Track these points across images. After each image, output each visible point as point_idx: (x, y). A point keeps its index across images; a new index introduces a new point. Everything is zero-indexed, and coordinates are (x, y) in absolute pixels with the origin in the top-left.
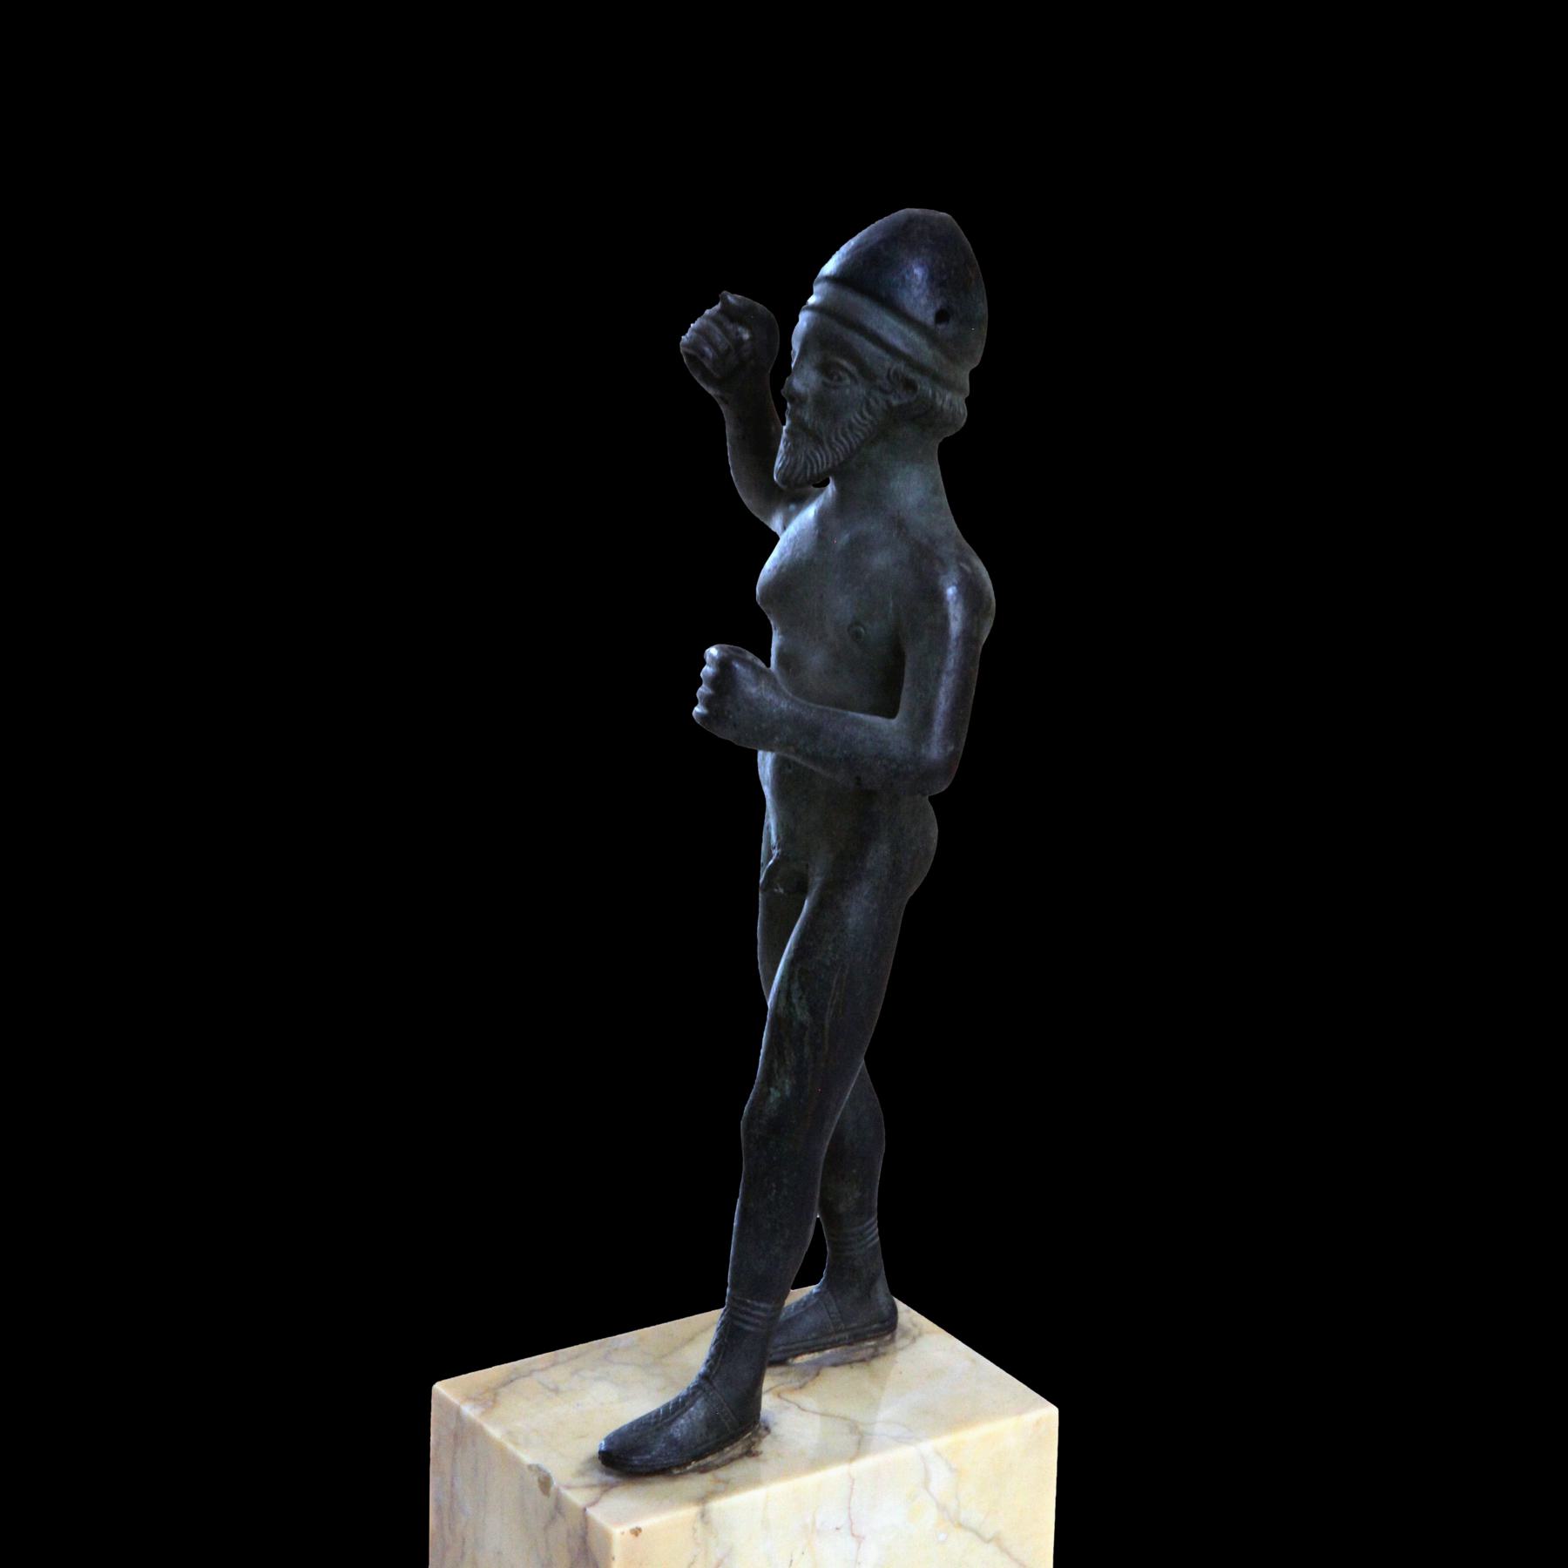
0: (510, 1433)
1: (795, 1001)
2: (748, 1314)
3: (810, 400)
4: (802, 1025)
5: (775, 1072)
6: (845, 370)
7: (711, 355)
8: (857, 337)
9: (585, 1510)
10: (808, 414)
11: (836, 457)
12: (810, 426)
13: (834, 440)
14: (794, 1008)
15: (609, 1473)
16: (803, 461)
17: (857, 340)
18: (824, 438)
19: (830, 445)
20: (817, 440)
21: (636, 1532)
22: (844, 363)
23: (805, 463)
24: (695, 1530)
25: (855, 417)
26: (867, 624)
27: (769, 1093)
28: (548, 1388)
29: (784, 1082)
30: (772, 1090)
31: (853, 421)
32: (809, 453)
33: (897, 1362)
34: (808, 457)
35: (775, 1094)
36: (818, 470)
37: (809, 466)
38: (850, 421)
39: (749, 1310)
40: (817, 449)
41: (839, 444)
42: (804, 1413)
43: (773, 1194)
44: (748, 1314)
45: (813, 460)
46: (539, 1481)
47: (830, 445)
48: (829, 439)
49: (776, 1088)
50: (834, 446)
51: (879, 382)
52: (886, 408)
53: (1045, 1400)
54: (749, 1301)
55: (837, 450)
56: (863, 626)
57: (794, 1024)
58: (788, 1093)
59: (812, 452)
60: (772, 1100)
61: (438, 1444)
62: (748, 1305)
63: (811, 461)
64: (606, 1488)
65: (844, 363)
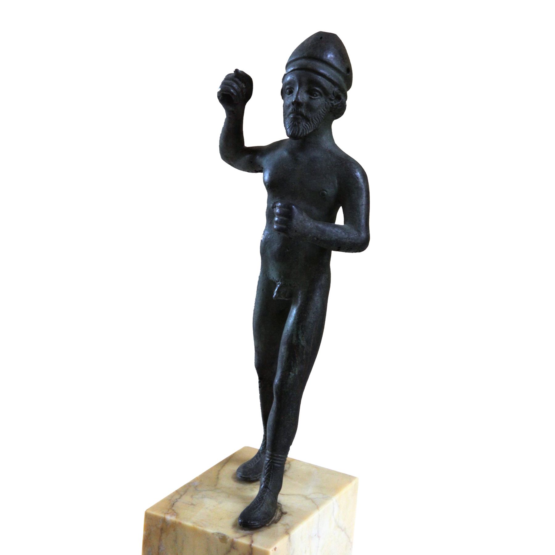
0: (194, 523)
1: (300, 337)
2: (280, 461)
3: (304, 104)
4: (303, 347)
5: (292, 366)
6: (318, 91)
7: (235, 94)
8: (320, 77)
9: (251, 545)
10: (303, 110)
11: (315, 126)
12: (305, 115)
13: (314, 120)
14: (300, 340)
16: (302, 128)
18: (310, 119)
19: (313, 122)
21: (275, 549)
22: (318, 89)
23: (303, 130)
24: (287, 545)
26: (328, 190)
27: (289, 374)
29: (295, 370)
30: (291, 373)
31: (321, 112)
32: (304, 125)
33: (286, 470)
34: (303, 127)
35: (292, 374)
36: (306, 133)
37: (305, 131)
38: (319, 112)
39: (280, 459)
40: (307, 123)
41: (315, 121)
42: (284, 496)
43: (290, 413)
44: (280, 461)
45: (306, 127)
46: (219, 538)
47: (313, 122)
48: (312, 119)
49: (292, 372)
50: (314, 122)
51: (330, 96)
52: (331, 106)
54: (280, 455)
55: (315, 123)
56: (326, 191)
57: (300, 347)
58: (297, 373)
59: (305, 125)
60: (290, 377)
62: (279, 457)
63: (305, 128)
64: (252, 534)
65: (318, 89)
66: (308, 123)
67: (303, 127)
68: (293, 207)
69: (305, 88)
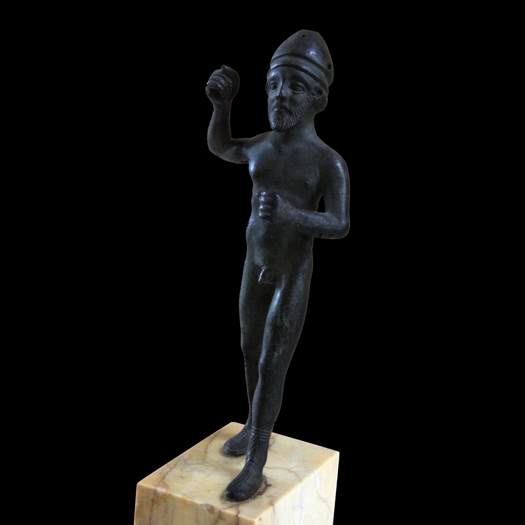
0: (184, 495)
1: (284, 319)
2: (265, 436)
3: (288, 99)
4: (287, 328)
5: (276, 346)
6: (300, 86)
8: (303, 73)
9: (237, 516)
10: (287, 104)
11: (298, 119)
12: (288, 109)
13: (297, 113)
14: (284, 322)
15: (232, 501)
16: (286, 121)
17: (302, 74)
18: (294, 113)
19: (296, 115)
20: (290, 113)
21: (260, 519)
22: (300, 84)
23: (287, 123)
24: (272, 515)
25: (304, 105)
26: (310, 180)
27: (274, 354)
28: (179, 477)
29: (279, 350)
30: (275, 353)
31: (304, 106)
32: (288, 119)
34: (287, 120)
35: (276, 354)
36: (289, 126)
37: (288, 124)
38: (302, 106)
39: (264, 434)
40: (290, 117)
41: (298, 114)
42: (268, 469)
43: (275, 391)
44: (265, 436)
45: (289, 121)
46: (208, 509)
47: (296, 115)
48: (295, 113)
49: (277, 352)
50: (297, 115)
51: (312, 91)
53: (326, 448)
54: (265, 431)
55: (298, 117)
56: (308, 181)
58: (281, 353)
59: (289, 119)
60: (275, 357)
61: (141, 506)
62: (264, 432)
63: (289, 121)
64: (238, 505)
65: (300, 84)
66: (292, 116)
67: (287, 120)
68: (278, 195)
69: (288, 83)
